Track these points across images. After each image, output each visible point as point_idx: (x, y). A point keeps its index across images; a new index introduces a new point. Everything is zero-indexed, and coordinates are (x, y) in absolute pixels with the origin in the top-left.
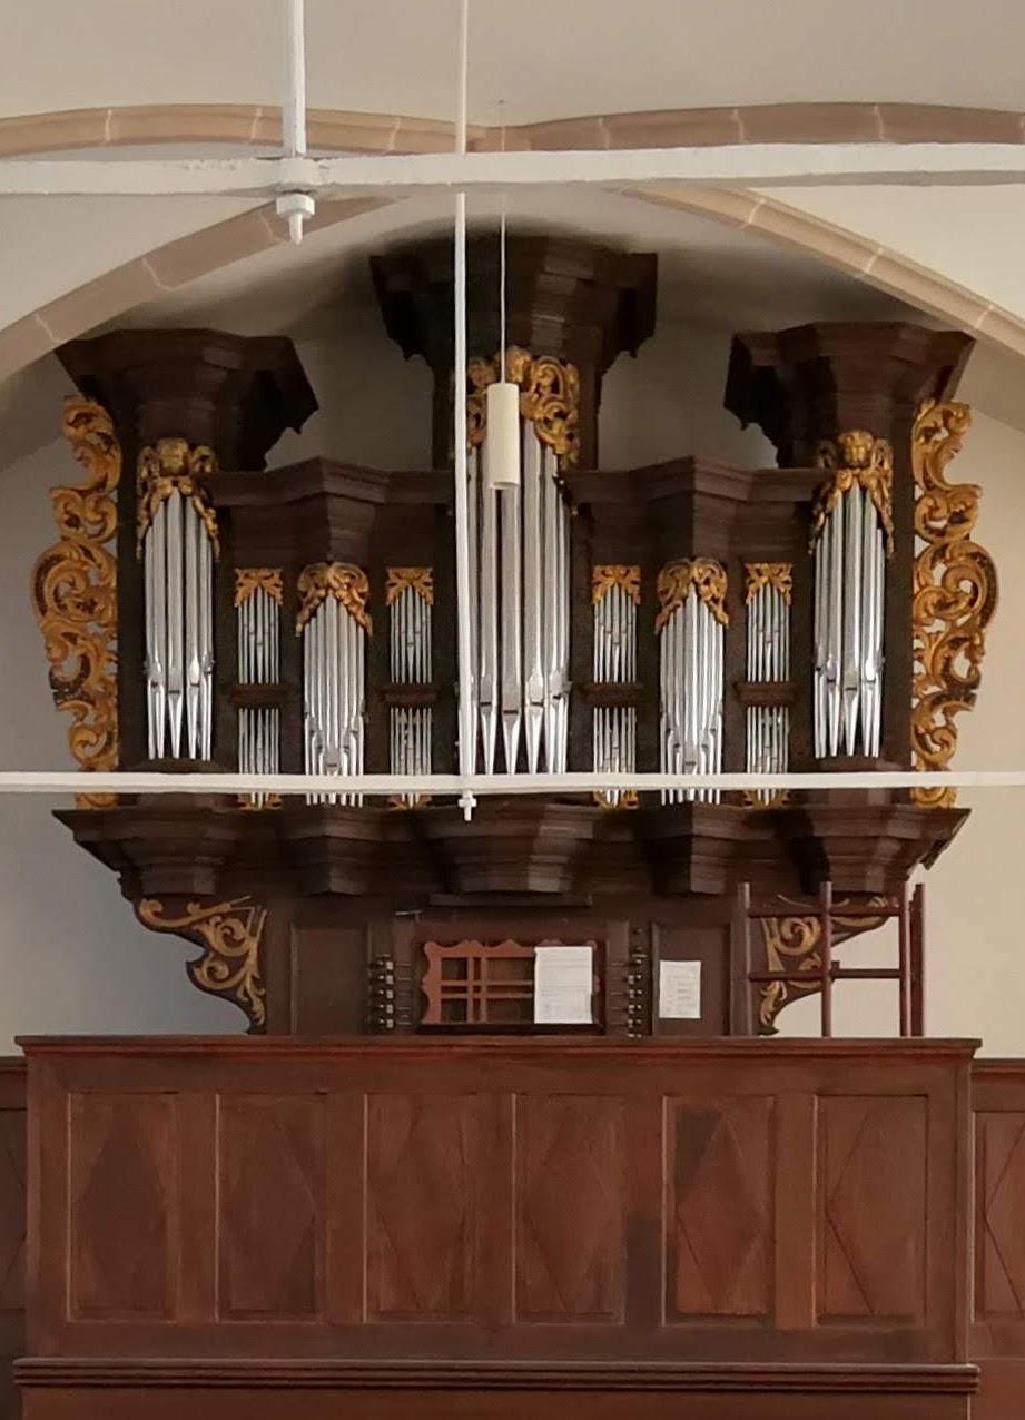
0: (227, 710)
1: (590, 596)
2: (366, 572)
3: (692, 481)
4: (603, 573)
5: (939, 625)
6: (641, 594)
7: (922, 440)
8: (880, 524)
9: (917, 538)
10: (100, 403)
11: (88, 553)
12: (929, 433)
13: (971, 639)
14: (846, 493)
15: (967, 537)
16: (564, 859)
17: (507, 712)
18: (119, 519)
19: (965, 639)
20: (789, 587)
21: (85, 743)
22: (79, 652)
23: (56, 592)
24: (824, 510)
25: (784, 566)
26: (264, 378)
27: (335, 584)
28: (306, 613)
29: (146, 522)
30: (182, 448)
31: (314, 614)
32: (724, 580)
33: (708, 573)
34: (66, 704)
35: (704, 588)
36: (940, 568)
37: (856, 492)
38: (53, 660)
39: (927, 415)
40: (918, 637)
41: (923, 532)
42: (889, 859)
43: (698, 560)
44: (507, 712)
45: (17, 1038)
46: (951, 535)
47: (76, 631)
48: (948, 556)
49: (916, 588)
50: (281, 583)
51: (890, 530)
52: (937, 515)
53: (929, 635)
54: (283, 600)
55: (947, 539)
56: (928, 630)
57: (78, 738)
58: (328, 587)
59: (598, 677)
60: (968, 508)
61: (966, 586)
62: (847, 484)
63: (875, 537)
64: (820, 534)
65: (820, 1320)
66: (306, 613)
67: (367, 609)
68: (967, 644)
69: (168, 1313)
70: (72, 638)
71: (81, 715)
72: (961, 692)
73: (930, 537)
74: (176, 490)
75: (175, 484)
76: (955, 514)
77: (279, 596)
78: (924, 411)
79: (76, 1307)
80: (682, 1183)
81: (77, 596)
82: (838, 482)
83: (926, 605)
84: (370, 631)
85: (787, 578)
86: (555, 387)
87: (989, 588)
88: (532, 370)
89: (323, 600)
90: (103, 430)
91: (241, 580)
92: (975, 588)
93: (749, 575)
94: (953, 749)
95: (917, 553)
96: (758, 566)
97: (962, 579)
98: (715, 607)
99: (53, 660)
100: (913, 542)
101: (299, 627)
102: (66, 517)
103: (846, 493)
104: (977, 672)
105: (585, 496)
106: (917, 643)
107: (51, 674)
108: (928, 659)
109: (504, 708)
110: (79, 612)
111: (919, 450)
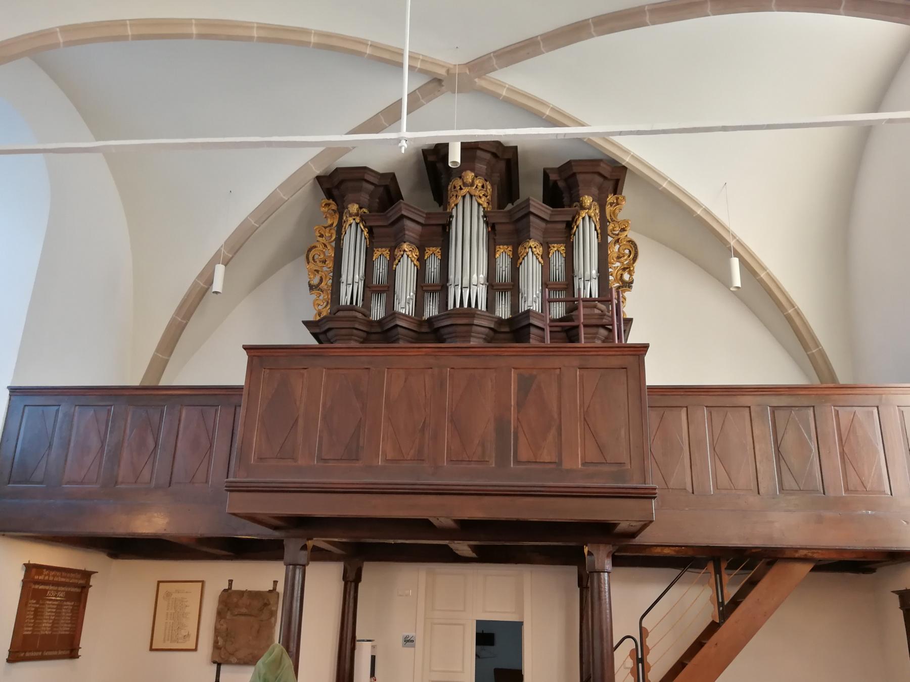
0: (368, 293)
1: (495, 255)
2: (418, 248)
3: (529, 207)
4: (499, 248)
5: (618, 264)
6: (513, 254)
7: (609, 206)
8: (596, 229)
9: (609, 237)
10: (333, 201)
11: (325, 246)
12: (611, 204)
13: (629, 268)
14: (583, 218)
15: (626, 236)
16: (484, 336)
17: (464, 288)
18: (336, 235)
19: (627, 268)
20: (564, 251)
21: (319, 305)
22: (319, 276)
23: (313, 257)
24: (576, 224)
25: (562, 245)
26: (386, 188)
27: (406, 250)
28: (397, 261)
29: (344, 233)
30: (356, 206)
31: (399, 261)
32: (541, 249)
33: (536, 245)
34: (313, 292)
35: (534, 249)
36: (617, 246)
37: (587, 218)
38: (310, 278)
39: (611, 198)
40: (610, 268)
41: (611, 234)
42: (604, 338)
43: (532, 240)
44: (464, 288)
45: (243, 346)
46: (621, 235)
47: (319, 269)
48: (620, 242)
49: (609, 252)
50: (389, 253)
51: (599, 231)
52: (615, 229)
53: (615, 267)
54: (389, 258)
55: (619, 237)
56: (614, 265)
57: (317, 302)
58: (404, 251)
59: (497, 280)
60: (626, 227)
61: (627, 251)
62: (584, 215)
63: (594, 234)
64: (574, 234)
65: (583, 464)
66: (397, 261)
67: (418, 260)
68: (628, 269)
69: (294, 459)
70: (317, 271)
71: (318, 296)
72: (628, 285)
73: (614, 236)
74: (354, 221)
75: (354, 219)
76: (622, 229)
77: (388, 257)
78: (610, 197)
79: (256, 458)
80: (520, 405)
81: (321, 259)
82: (581, 215)
83: (613, 257)
84: (419, 267)
85: (563, 248)
86: (483, 187)
87: (635, 251)
88: (475, 180)
89: (402, 256)
90: (333, 208)
91: (376, 251)
92: (630, 251)
93: (550, 248)
94: (625, 304)
95: (609, 242)
96: (553, 245)
97: (625, 249)
98: (538, 257)
99: (310, 278)
100: (607, 238)
101: (395, 266)
102: (319, 235)
103: (583, 218)
104: (632, 278)
105: (492, 221)
106: (610, 270)
107: (309, 282)
108: (614, 275)
109: (463, 286)
110: (321, 263)
111: (608, 209)
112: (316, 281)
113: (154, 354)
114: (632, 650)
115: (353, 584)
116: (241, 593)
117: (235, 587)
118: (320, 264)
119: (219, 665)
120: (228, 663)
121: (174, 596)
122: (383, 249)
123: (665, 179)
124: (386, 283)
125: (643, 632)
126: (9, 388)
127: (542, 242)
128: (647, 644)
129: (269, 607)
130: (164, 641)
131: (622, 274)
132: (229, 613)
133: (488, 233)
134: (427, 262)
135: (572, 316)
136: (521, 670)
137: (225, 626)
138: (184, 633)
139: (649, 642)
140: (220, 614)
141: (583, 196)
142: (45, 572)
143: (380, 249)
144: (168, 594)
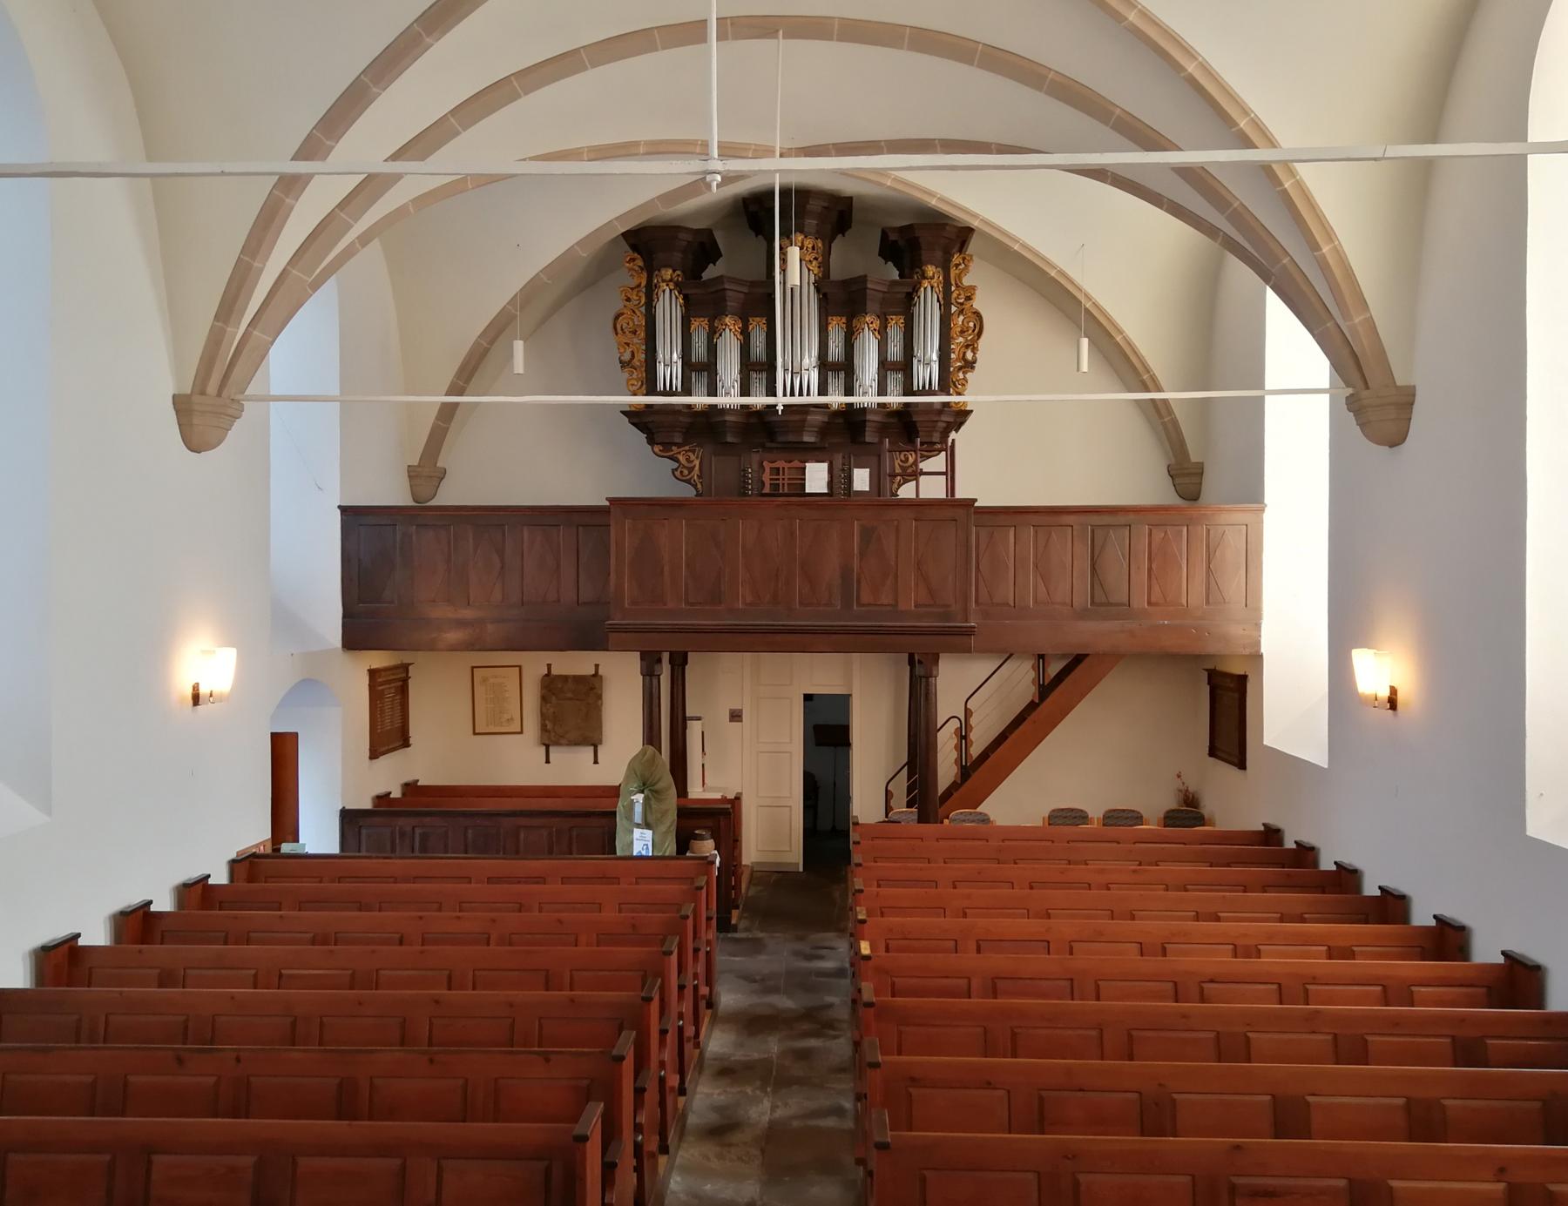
8: (938, 301)
11: (634, 312)
12: (957, 266)
14: (925, 289)
21: (633, 385)
30: (670, 271)
31: (721, 335)
36: (961, 318)
37: (929, 288)
39: (956, 259)
51: (942, 303)
58: (726, 325)
59: (830, 359)
61: (971, 324)
63: (936, 306)
65: (915, 607)
67: (741, 333)
70: (628, 344)
72: (969, 365)
75: (667, 285)
80: (862, 555)
86: (813, 248)
92: (975, 325)
99: (620, 353)
103: (925, 289)
105: (824, 291)
106: (953, 346)
108: (957, 353)
111: (953, 272)
112: (627, 357)
113: (434, 422)
114: (956, 729)
115: (681, 668)
116: (565, 678)
117: (554, 672)
118: (630, 335)
119: (547, 747)
120: (557, 744)
121: (492, 680)
122: (702, 319)
123: (1016, 241)
124: (706, 360)
125: (968, 713)
126: (339, 507)
127: (879, 314)
128: (971, 723)
129: (595, 691)
130: (487, 725)
131: (965, 353)
132: (554, 698)
133: (819, 300)
134: (752, 334)
135: (908, 412)
136: (848, 726)
137: (552, 710)
138: (506, 716)
139: (973, 721)
140: (544, 699)
141: (926, 265)
142: (383, 673)
143: (697, 320)
144: (485, 680)
